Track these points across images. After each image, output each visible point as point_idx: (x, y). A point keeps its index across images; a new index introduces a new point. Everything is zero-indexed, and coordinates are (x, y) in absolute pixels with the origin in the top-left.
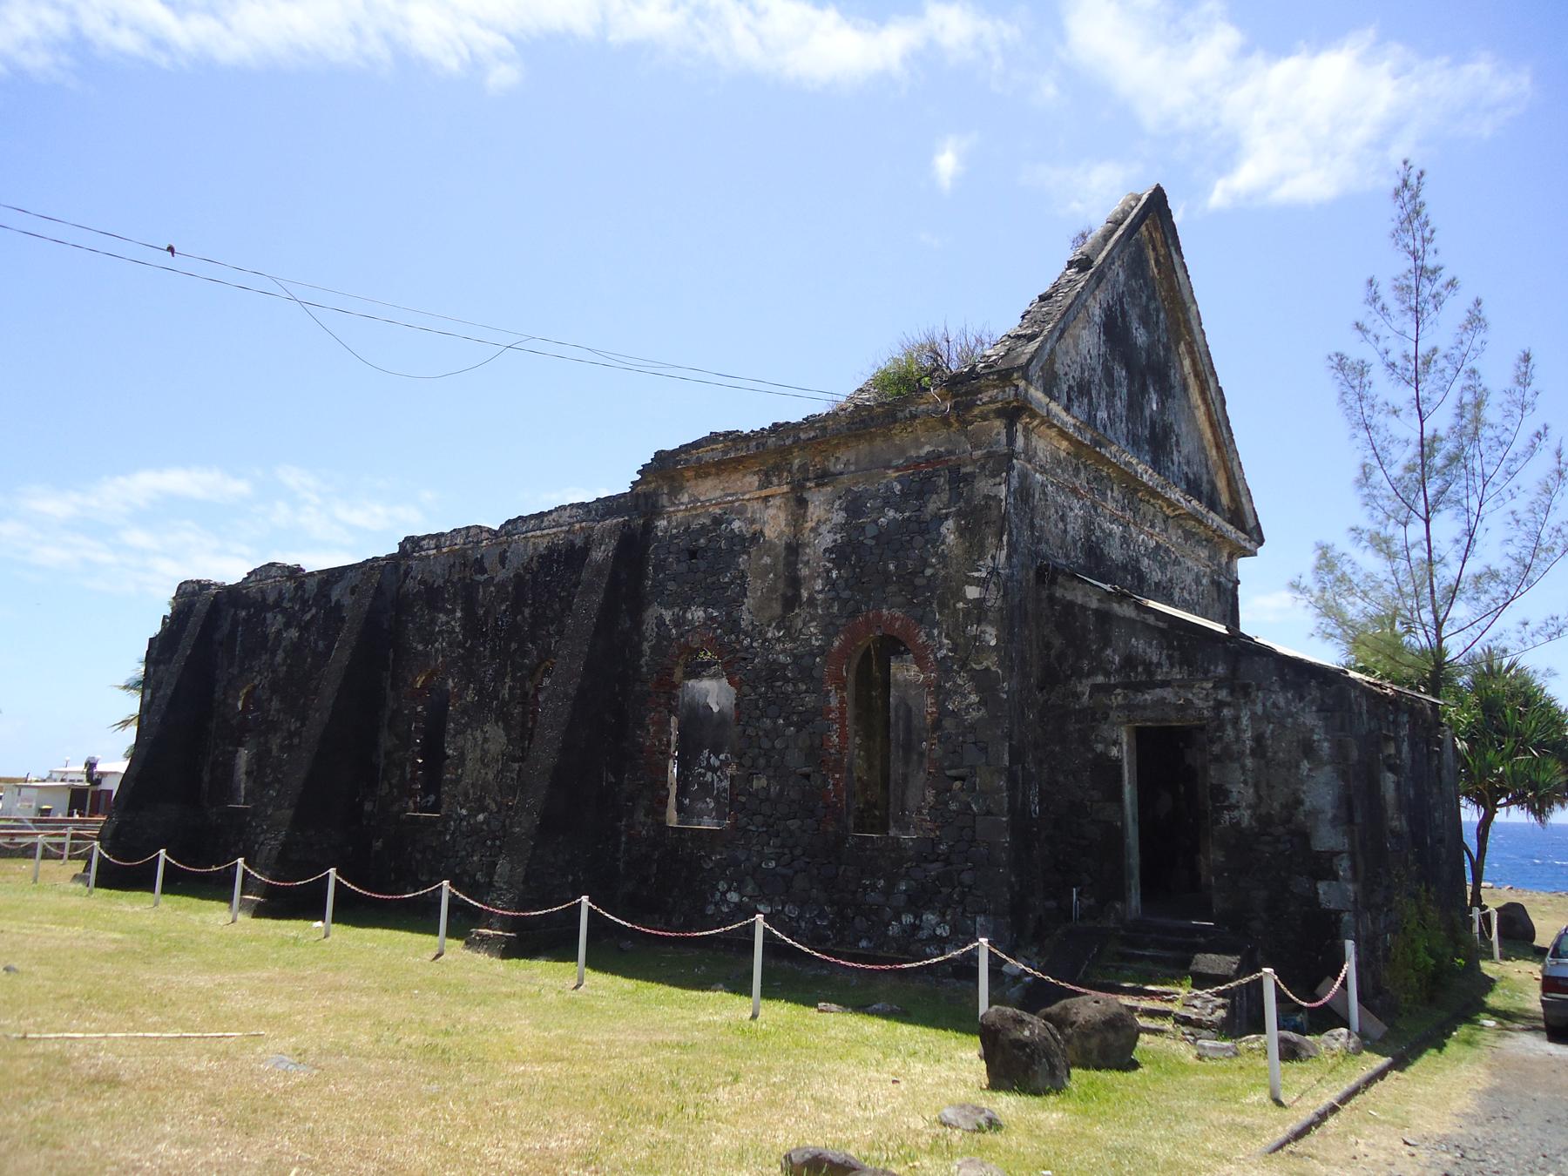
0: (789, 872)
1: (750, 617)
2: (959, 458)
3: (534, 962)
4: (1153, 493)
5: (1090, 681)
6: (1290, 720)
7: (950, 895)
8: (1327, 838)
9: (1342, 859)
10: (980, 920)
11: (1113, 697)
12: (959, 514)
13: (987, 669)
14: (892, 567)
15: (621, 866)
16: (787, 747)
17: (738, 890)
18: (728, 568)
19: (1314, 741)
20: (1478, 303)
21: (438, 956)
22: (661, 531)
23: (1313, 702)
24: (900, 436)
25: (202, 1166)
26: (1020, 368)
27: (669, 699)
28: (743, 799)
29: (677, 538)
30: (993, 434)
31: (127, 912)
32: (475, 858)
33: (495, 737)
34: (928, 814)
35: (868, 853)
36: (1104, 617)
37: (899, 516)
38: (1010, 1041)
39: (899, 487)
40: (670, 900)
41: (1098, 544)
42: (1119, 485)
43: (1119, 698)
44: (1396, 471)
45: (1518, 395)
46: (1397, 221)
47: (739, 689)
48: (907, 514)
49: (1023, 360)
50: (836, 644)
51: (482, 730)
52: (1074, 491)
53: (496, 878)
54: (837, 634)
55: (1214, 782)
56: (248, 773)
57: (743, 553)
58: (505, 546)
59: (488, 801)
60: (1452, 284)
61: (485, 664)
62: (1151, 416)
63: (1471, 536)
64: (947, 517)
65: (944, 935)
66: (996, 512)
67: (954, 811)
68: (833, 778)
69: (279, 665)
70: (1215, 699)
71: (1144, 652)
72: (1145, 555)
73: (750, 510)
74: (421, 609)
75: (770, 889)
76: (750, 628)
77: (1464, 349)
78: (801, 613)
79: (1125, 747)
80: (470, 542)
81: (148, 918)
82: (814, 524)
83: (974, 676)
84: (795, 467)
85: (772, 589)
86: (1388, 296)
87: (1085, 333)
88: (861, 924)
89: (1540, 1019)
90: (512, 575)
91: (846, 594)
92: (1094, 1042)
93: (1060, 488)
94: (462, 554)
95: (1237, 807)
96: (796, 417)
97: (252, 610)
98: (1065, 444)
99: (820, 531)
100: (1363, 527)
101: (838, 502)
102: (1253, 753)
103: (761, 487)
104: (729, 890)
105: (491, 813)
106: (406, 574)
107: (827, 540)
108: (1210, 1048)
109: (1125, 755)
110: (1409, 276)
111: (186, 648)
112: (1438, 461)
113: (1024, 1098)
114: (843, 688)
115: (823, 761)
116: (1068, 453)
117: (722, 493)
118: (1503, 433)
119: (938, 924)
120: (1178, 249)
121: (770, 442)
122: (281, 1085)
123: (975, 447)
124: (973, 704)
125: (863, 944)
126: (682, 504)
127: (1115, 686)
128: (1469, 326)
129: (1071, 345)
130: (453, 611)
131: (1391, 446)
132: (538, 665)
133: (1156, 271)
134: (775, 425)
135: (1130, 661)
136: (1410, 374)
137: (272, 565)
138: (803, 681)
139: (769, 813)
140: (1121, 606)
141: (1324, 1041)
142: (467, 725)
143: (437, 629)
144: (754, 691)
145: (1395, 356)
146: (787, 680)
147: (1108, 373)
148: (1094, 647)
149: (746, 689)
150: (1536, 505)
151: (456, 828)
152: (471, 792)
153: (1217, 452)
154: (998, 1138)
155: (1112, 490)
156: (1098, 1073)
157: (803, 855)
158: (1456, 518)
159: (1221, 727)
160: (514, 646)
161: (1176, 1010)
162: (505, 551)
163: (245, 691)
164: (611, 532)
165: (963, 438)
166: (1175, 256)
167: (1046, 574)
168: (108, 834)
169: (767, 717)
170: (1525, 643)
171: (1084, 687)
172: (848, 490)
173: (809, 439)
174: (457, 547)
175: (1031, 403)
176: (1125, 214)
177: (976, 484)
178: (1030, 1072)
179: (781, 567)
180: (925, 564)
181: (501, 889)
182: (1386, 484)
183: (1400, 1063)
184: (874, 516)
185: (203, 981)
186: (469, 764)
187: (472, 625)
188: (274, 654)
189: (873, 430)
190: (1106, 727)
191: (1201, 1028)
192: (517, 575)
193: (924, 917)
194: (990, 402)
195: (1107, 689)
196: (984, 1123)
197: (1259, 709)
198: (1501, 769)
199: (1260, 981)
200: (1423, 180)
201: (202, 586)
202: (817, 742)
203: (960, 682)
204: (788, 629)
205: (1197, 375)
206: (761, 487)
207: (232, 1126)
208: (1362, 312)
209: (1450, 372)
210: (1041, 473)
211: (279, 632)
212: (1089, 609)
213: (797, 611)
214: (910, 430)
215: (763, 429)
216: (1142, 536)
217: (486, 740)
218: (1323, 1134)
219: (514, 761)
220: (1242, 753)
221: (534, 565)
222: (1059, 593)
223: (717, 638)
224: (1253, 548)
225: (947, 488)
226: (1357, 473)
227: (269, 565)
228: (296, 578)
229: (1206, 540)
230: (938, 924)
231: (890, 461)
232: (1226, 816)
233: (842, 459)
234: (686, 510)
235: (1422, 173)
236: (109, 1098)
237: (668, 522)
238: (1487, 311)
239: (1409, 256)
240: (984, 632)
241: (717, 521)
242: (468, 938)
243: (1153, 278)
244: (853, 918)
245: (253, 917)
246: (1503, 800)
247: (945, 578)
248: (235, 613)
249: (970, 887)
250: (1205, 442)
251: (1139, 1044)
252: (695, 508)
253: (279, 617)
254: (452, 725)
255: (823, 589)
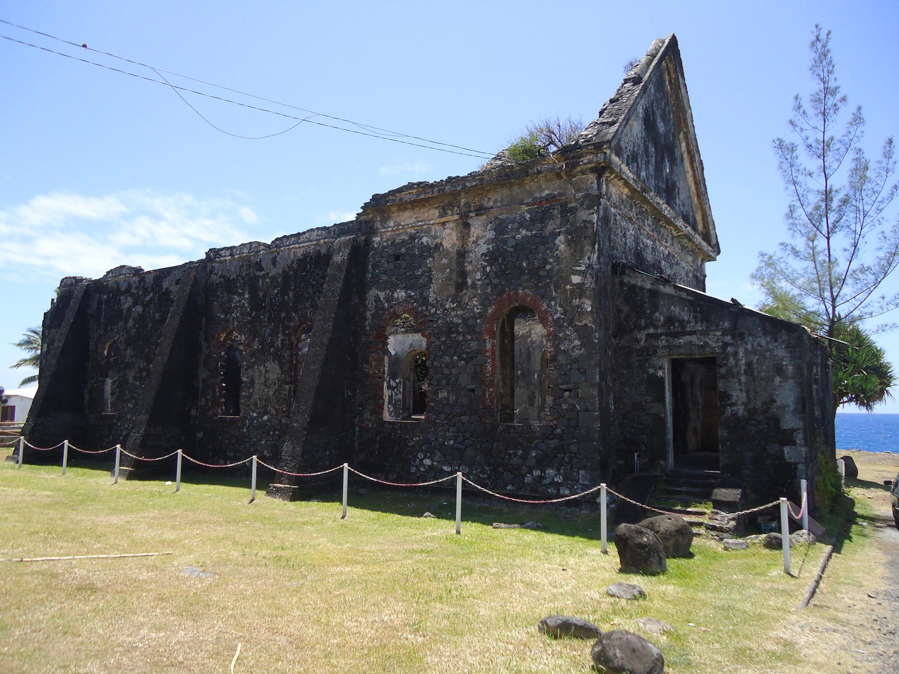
0: (463, 447)
1: (435, 296)
2: (567, 198)
3: (310, 503)
4: (669, 222)
5: (646, 332)
6: (768, 353)
7: (563, 458)
8: (790, 421)
9: (799, 433)
10: (582, 472)
11: (660, 341)
12: (567, 232)
13: (586, 325)
14: (524, 264)
15: (356, 445)
16: (460, 373)
17: (430, 458)
18: (420, 266)
19: (784, 365)
20: (859, 108)
21: (252, 500)
22: (377, 244)
23: (783, 342)
24: (530, 185)
25: (175, 644)
26: (609, 142)
27: (384, 346)
28: (433, 404)
29: (386, 248)
30: (589, 183)
31: (48, 479)
32: (263, 442)
33: (274, 370)
34: (549, 411)
35: (512, 434)
36: (654, 294)
37: (529, 234)
38: (635, 544)
39: (529, 216)
40: (388, 464)
41: (641, 251)
42: (651, 216)
43: (664, 341)
44: (809, 209)
45: (884, 164)
46: (813, 61)
47: (428, 339)
48: (534, 232)
49: (609, 137)
50: (490, 311)
51: (264, 366)
52: (630, 219)
53: (283, 454)
54: (490, 305)
55: (721, 390)
56: (112, 394)
57: (430, 257)
58: (276, 254)
59: (270, 408)
60: (843, 99)
61: (265, 326)
62: (666, 176)
63: (856, 247)
64: (559, 234)
65: (560, 481)
66: (591, 231)
67: (565, 409)
68: (489, 391)
69: (130, 328)
70: (723, 342)
71: (679, 314)
72: (662, 259)
73: (433, 230)
74: (222, 293)
75: (457, 458)
76: (435, 302)
77: (851, 136)
78: (467, 293)
79: (666, 371)
80: (252, 252)
81: (61, 482)
82: (474, 239)
83: (577, 329)
84: (462, 204)
85: (449, 278)
86: (807, 105)
87: (635, 123)
88: (507, 476)
89: (892, 521)
90: (280, 272)
91: (495, 281)
92: (671, 543)
93: (623, 217)
94: (248, 258)
95: (735, 404)
96: (463, 173)
97: (111, 295)
98: (626, 190)
99: (478, 243)
100: (787, 243)
101: (490, 225)
102: (746, 372)
103: (441, 216)
104: (425, 458)
105: (272, 415)
106: (211, 272)
107: (483, 248)
108: (732, 543)
109: (666, 375)
110: (820, 93)
111: (69, 317)
112: (835, 204)
113: (646, 577)
114: (494, 338)
115: (482, 381)
116: (627, 196)
117: (415, 220)
118: (876, 186)
119: (556, 475)
120: (683, 74)
121: (447, 188)
122: (199, 586)
123: (577, 191)
124: (577, 346)
125: (510, 487)
126: (390, 227)
127: (661, 334)
128: (854, 123)
129: (629, 131)
130: (243, 294)
131: (809, 193)
132: (299, 326)
133: (669, 88)
134: (449, 178)
135: (670, 320)
136: (820, 152)
137: (123, 267)
138: (469, 334)
139: (449, 413)
140: (665, 287)
141: (794, 538)
142: (254, 363)
143: (233, 305)
144: (438, 340)
145: (811, 141)
146: (459, 333)
147: (646, 148)
148: (648, 312)
149: (433, 339)
150: (896, 228)
151: (250, 425)
152: (259, 403)
153: (698, 199)
154: (647, 603)
155: (648, 220)
156: (674, 560)
157: (471, 436)
158: (846, 236)
159: (726, 357)
160: (283, 315)
161: (706, 522)
162: (276, 257)
163: (108, 344)
164: (345, 244)
165: (569, 186)
166: (681, 79)
167: (618, 269)
168: (27, 431)
169: (447, 355)
170: (882, 309)
171: (642, 336)
172: (496, 218)
173: (472, 187)
174: (244, 255)
175: (612, 164)
176: (657, 51)
177: (577, 213)
178: (648, 562)
179: (454, 264)
180: (546, 262)
181: (287, 460)
182: (804, 217)
183: (837, 549)
184: (513, 234)
185: (115, 520)
186: (257, 386)
187: (256, 303)
188: (126, 322)
189: (513, 181)
190: (655, 358)
191: (723, 532)
192: (284, 272)
193: (547, 472)
194: (588, 163)
195: (656, 336)
196: (636, 593)
197: (749, 347)
198: (846, 382)
199: (778, 506)
200: (830, 36)
201: (77, 281)
202: (479, 370)
203: (568, 333)
204: (459, 303)
205: (689, 153)
206: (441, 216)
207: (182, 615)
208: (792, 115)
209: (843, 150)
210: (614, 208)
211: (130, 308)
212: (645, 289)
213: (464, 291)
214: (536, 180)
215: (442, 180)
216: (662, 248)
217: (267, 372)
218: (822, 592)
219: (286, 383)
220: (739, 373)
221: (295, 265)
222: (626, 280)
223: (414, 308)
224: (714, 256)
225: (559, 216)
226: (787, 210)
227: (121, 267)
228: (139, 275)
229: (691, 251)
230: (556, 475)
231: (523, 200)
232: (729, 410)
233: (492, 199)
234: (392, 231)
235: (829, 33)
236: (94, 600)
237: (381, 238)
238: (865, 113)
239: (820, 82)
240: (583, 303)
241: (412, 238)
242: (267, 490)
243: (668, 92)
244: (503, 473)
245: (127, 480)
246: (845, 399)
247: (559, 271)
248: (100, 297)
249: (575, 453)
250: (692, 194)
251: (693, 543)
252: (398, 230)
253: (129, 299)
254: (245, 363)
255: (481, 279)
